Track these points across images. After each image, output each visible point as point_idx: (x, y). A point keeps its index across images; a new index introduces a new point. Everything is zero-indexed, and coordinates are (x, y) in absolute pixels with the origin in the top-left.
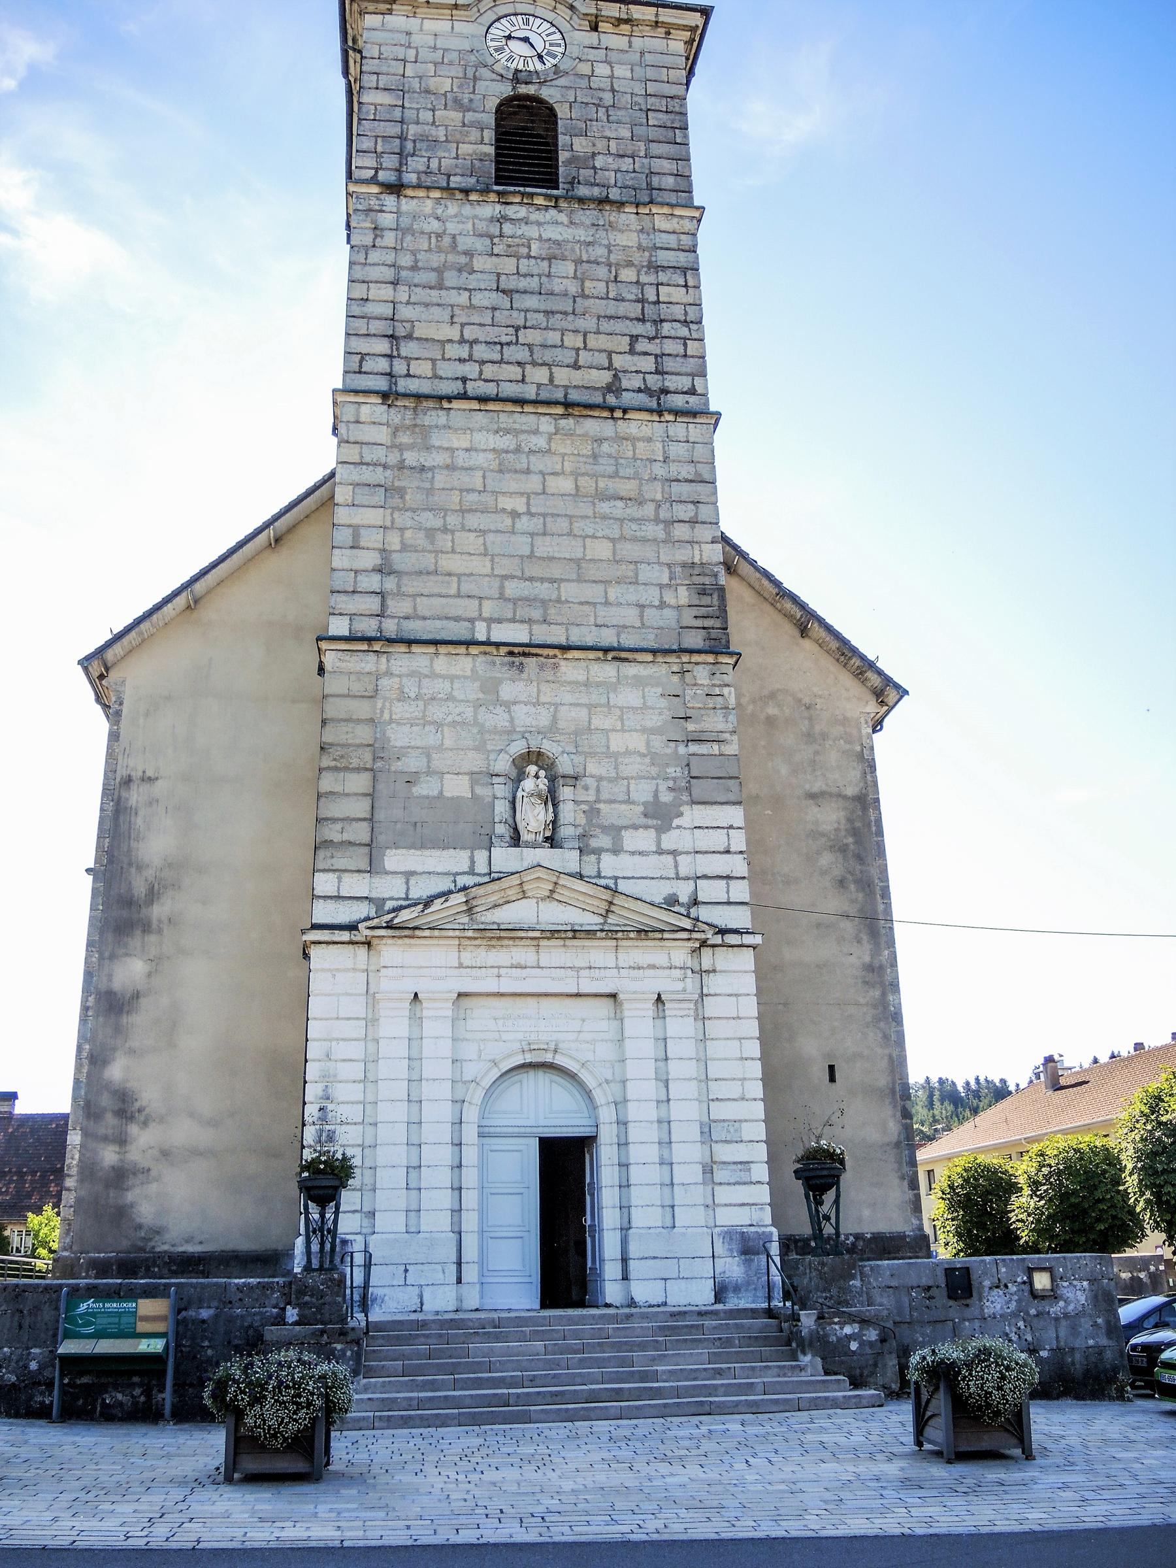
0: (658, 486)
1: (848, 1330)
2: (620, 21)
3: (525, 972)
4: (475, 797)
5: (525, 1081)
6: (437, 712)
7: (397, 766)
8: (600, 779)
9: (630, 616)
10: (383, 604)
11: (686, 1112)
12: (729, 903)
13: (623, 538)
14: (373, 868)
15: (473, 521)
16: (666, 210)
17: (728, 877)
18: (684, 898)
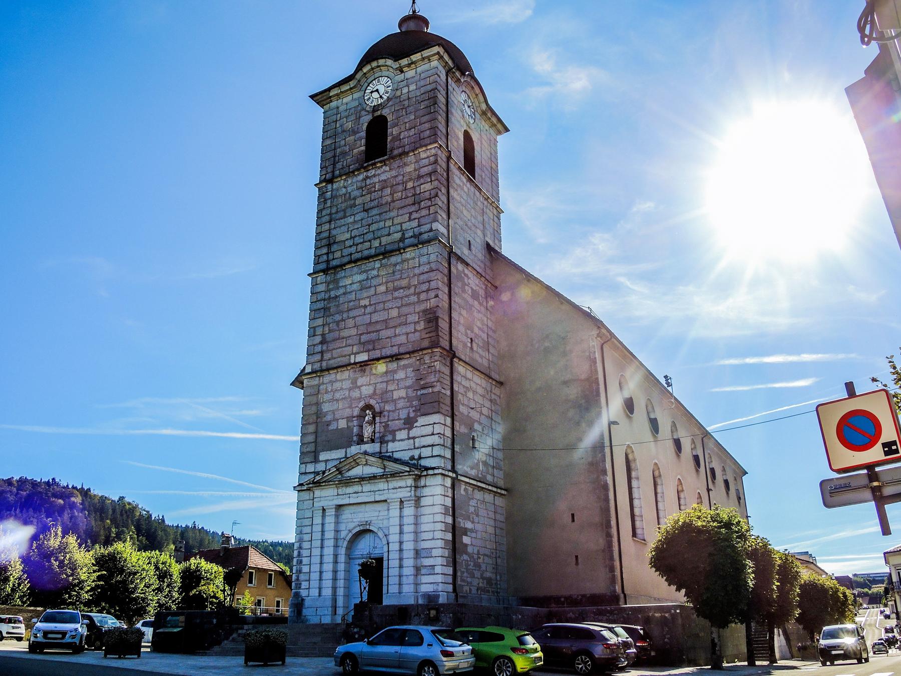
1: (355, 630)
2: (409, 65)
4: (348, 427)
6: (338, 395)
7: (325, 419)
8: (389, 411)
9: (403, 339)
10: (322, 356)
11: (409, 546)
12: (432, 456)
13: (402, 305)
14: (316, 460)
15: (352, 314)
16: (424, 149)
17: (433, 445)
18: (416, 457)
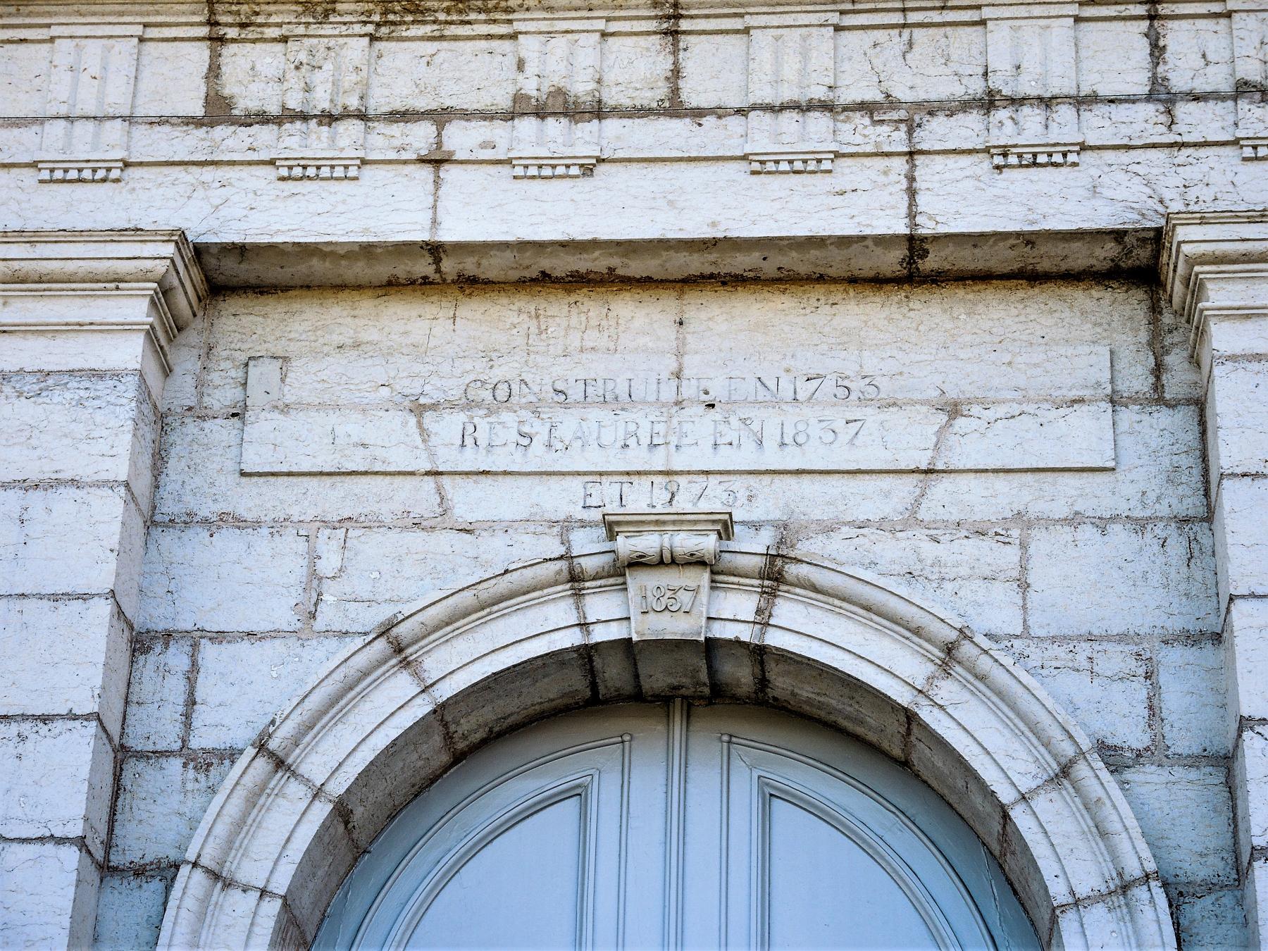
0: (1249, 27)
3: (586, 138)
5: (606, 793)
